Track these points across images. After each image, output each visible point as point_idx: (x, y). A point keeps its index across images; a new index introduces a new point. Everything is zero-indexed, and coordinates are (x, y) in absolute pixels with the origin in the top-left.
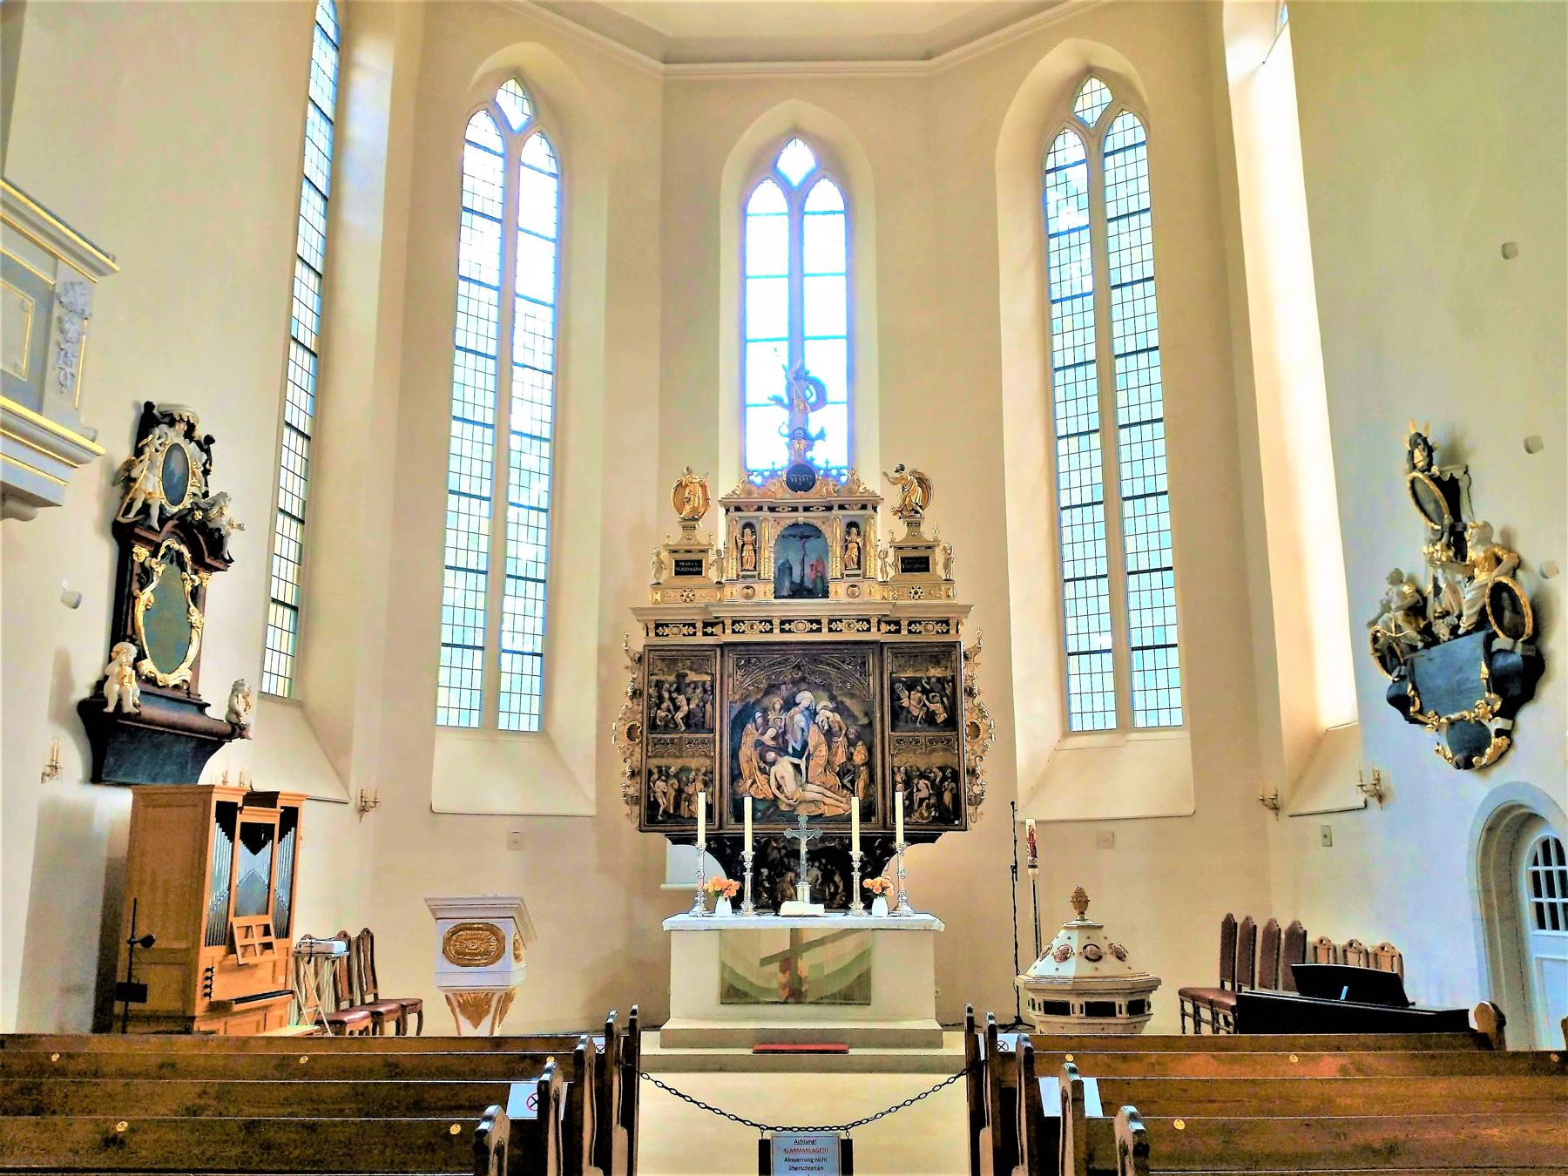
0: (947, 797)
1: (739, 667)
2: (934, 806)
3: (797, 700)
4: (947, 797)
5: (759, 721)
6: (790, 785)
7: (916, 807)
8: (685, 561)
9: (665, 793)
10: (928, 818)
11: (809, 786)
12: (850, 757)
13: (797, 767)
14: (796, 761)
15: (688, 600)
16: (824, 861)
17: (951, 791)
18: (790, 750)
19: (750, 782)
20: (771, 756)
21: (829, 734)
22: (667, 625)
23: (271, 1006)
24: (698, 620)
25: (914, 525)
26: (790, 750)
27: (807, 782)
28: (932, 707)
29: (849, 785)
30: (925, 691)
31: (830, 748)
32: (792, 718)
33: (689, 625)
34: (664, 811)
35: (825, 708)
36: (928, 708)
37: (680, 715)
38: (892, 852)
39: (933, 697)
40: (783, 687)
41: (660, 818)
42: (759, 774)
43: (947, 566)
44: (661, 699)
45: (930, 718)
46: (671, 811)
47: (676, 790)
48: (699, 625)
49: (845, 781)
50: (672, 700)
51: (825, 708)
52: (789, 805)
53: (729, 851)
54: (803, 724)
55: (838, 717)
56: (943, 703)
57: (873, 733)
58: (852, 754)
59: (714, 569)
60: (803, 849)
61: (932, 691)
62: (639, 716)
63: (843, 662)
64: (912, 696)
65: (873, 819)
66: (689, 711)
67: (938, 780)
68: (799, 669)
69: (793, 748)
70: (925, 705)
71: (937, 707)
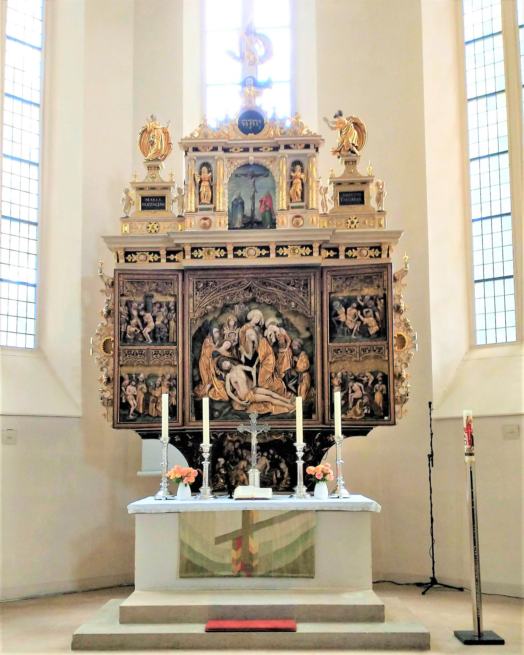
4: (378, 397)
6: (243, 389)
7: (351, 405)
8: (150, 198)
9: (135, 396)
11: (259, 390)
12: (294, 366)
13: (248, 374)
14: (248, 368)
16: (271, 451)
17: (381, 391)
18: (243, 359)
19: (209, 386)
20: (226, 364)
21: (276, 345)
22: (135, 253)
25: (351, 163)
26: (243, 359)
28: (366, 320)
29: (293, 388)
30: (359, 308)
32: (244, 333)
33: (155, 253)
34: (135, 411)
35: (273, 323)
36: (362, 322)
38: (331, 443)
39: (367, 312)
40: (236, 306)
41: (131, 417)
43: (379, 200)
44: (130, 316)
45: (364, 331)
48: (163, 253)
49: (290, 385)
50: (141, 317)
51: (273, 323)
52: (243, 406)
54: (254, 337)
55: (284, 332)
56: (375, 316)
57: (313, 345)
58: (296, 362)
59: (175, 204)
60: (254, 442)
61: (366, 307)
63: (288, 284)
64: (348, 312)
65: (313, 416)
66: (155, 327)
67: (370, 382)
68: (250, 291)
69: (246, 358)
70: (359, 319)
71: (370, 321)
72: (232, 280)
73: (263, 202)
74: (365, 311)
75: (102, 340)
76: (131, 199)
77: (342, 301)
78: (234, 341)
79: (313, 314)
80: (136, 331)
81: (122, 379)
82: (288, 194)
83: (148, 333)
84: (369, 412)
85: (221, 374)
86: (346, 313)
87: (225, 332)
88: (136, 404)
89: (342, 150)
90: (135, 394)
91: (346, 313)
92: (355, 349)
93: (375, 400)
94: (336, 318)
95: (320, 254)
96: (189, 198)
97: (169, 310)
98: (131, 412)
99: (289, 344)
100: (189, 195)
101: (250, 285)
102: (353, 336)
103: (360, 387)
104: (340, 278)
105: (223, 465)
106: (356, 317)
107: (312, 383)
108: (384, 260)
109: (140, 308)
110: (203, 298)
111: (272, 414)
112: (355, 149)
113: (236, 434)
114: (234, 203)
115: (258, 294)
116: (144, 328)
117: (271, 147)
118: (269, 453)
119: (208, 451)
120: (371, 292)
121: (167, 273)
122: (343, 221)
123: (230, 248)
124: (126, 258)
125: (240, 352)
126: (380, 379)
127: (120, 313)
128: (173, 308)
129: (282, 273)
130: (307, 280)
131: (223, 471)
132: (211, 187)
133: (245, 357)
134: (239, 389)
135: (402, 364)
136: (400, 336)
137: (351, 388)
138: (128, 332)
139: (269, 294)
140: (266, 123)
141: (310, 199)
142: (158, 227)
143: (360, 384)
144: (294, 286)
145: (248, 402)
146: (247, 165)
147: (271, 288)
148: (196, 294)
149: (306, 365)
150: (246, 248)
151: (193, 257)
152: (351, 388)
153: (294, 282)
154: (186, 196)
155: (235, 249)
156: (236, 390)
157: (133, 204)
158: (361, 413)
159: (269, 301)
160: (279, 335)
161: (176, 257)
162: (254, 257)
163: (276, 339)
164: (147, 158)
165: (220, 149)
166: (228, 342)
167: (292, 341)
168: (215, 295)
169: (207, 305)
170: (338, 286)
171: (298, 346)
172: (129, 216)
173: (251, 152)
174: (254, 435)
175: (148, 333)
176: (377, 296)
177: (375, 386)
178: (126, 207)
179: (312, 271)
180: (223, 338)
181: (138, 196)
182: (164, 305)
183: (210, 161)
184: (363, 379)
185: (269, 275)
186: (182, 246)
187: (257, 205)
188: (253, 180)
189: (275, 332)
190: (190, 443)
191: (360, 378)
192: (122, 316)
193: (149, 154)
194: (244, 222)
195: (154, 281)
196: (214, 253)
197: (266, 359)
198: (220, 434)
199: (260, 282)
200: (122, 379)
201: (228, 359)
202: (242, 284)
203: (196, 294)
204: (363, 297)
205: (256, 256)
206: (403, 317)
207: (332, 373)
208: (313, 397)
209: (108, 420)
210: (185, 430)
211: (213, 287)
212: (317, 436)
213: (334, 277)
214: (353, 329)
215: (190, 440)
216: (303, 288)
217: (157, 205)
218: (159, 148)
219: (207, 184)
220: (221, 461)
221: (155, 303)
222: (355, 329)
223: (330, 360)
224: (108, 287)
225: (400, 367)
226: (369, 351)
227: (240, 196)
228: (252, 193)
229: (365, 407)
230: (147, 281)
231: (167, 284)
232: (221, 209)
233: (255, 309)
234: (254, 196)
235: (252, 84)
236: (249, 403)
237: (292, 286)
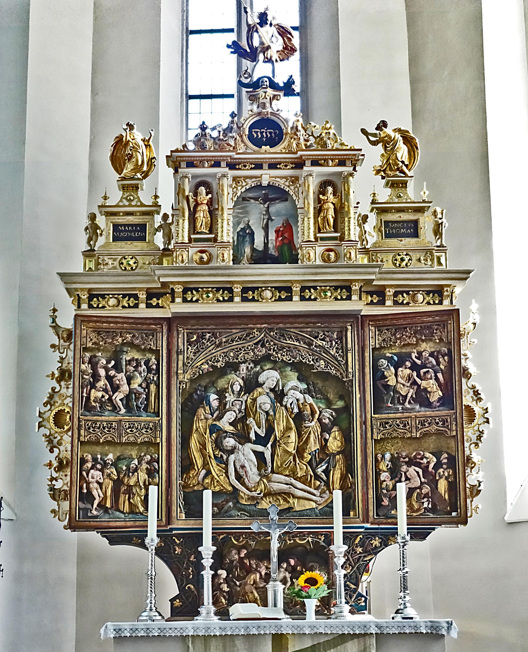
0: (442, 486)
1: (190, 343)
2: (426, 496)
3: (261, 379)
4: (442, 486)
5: (215, 404)
8: (125, 225)
9: (100, 484)
10: (418, 510)
12: (324, 447)
13: (260, 456)
14: (259, 448)
15: (129, 268)
16: (292, 562)
17: (447, 478)
18: (252, 436)
19: (204, 472)
20: (230, 442)
22: (103, 296)
23: (252, 450)
24: (140, 289)
26: (252, 436)
27: (273, 472)
28: (424, 384)
29: (324, 476)
30: (414, 367)
31: (299, 435)
32: (254, 400)
33: (130, 296)
35: (295, 388)
36: (419, 386)
37: (118, 397)
39: (425, 373)
40: (243, 367)
41: (95, 512)
42: (214, 462)
44: (96, 377)
46: (108, 505)
47: (114, 481)
48: (142, 296)
49: (319, 471)
51: (295, 388)
52: (253, 498)
53: (178, 550)
54: (267, 407)
55: (310, 400)
56: (437, 379)
57: (350, 417)
58: (326, 441)
59: (159, 235)
60: (275, 545)
61: (424, 366)
62: (69, 400)
63: (316, 338)
64: (400, 373)
65: (352, 513)
66: (131, 391)
67: (431, 466)
68: (263, 346)
70: (415, 383)
71: (430, 384)
72: (238, 331)
73: (280, 233)
74: (422, 371)
75: (52, 411)
76: (98, 227)
77: (390, 360)
78: (240, 411)
79: (351, 376)
80: (103, 396)
81: (83, 461)
82: (316, 222)
83: (120, 400)
84: (430, 506)
85: (221, 456)
86: (396, 375)
87: (227, 400)
88: (102, 495)
89: (388, 169)
90: (101, 481)
91: (396, 375)
92: (410, 422)
93: (439, 490)
94: (382, 382)
95: (360, 299)
96: (181, 226)
97: (149, 370)
98: (95, 506)
99: (317, 416)
100: (181, 221)
101: (262, 338)
102: (407, 405)
103: (418, 473)
104: (387, 330)
105: (225, 579)
106: (409, 379)
107: (349, 468)
108: (446, 305)
109: (110, 366)
110: (197, 355)
111: (294, 510)
112: (404, 168)
113: (244, 536)
114: (241, 233)
115: (274, 350)
116: (113, 394)
117: (292, 164)
118: (289, 563)
119: (211, 556)
120: (430, 347)
121: (148, 322)
122: (391, 256)
123: (237, 289)
124: (91, 303)
125: (247, 425)
126: (445, 461)
127: (83, 372)
128: (154, 367)
129: (307, 324)
130: (341, 332)
131: (225, 588)
132: (210, 212)
133: (255, 432)
134: (246, 476)
135: (471, 444)
136: (468, 407)
137: (405, 473)
138: (92, 398)
139: (289, 350)
140: (286, 134)
141: (346, 228)
142: (135, 263)
143: (417, 469)
144: (323, 340)
145: (260, 494)
146: (259, 187)
147: (292, 343)
148: (188, 349)
149: (340, 444)
150: (260, 289)
151: (185, 300)
152: (405, 473)
153: (324, 334)
154: (175, 223)
155: (245, 290)
156: (242, 477)
157: (101, 235)
158: (420, 507)
159: (288, 359)
160: (302, 404)
161: (160, 302)
162: (270, 301)
163: (299, 408)
164: (122, 175)
165: (223, 164)
166: (232, 412)
167: (321, 412)
168: (214, 351)
169: (202, 364)
170: (384, 340)
171: (329, 418)
172: (96, 249)
173: (265, 170)
174: (275, 535)
175: (120, 400)
176: (439, 352)
177: (438, 472)
178: (90, 239)
179: (349, 320)
180: (225, 408)
181: (109, 223)
182: (142, 363)
183: (209, 180)
184: (421, 461)
185: (288, 325)
186: (171, 286)
187: (272, 236)
188: (266, 206)
189: (298, 400)
190: (177, 549)
191: (418, 460)
192: (85, 376)
193: (125, 171)
194: (254, 258)
195: (130, 331)
196: (214, 295)
197: (285, 436)
198: (221, 537)
199: (276, 334)
200: (83, 461)
201: (233, 435)
202: (251, 336)
203: (188, 349)
204: (420, 354)
205: (273, 300)
206: (471, 382)
207: (377, 454)
208: (351, 487)
209: (59, 519)
210: (172, 530)
211: (211, 339)
212: (358, 539)
213: (379, 328)
214: (406, 396)
215: (178, 545)
216: (336, 343)
217: (135, 234)
218: (140, 163)
219: (206, 208)
220: (223, 573)
221: (130, 361)
222: (410, 395)
223: (375, 437)
224: (62, 341)
225: (468, 448)
226: (429, 424)
227: (248, 225)
228: (265, 221)
229: (426, 499)
230: (120, 330)
231: (146, 336)
232: (225, 239)
233: (268, 369)
234: (267, 225)
235: (268, 85)
236: (262, 495)
237: (320, 340)
